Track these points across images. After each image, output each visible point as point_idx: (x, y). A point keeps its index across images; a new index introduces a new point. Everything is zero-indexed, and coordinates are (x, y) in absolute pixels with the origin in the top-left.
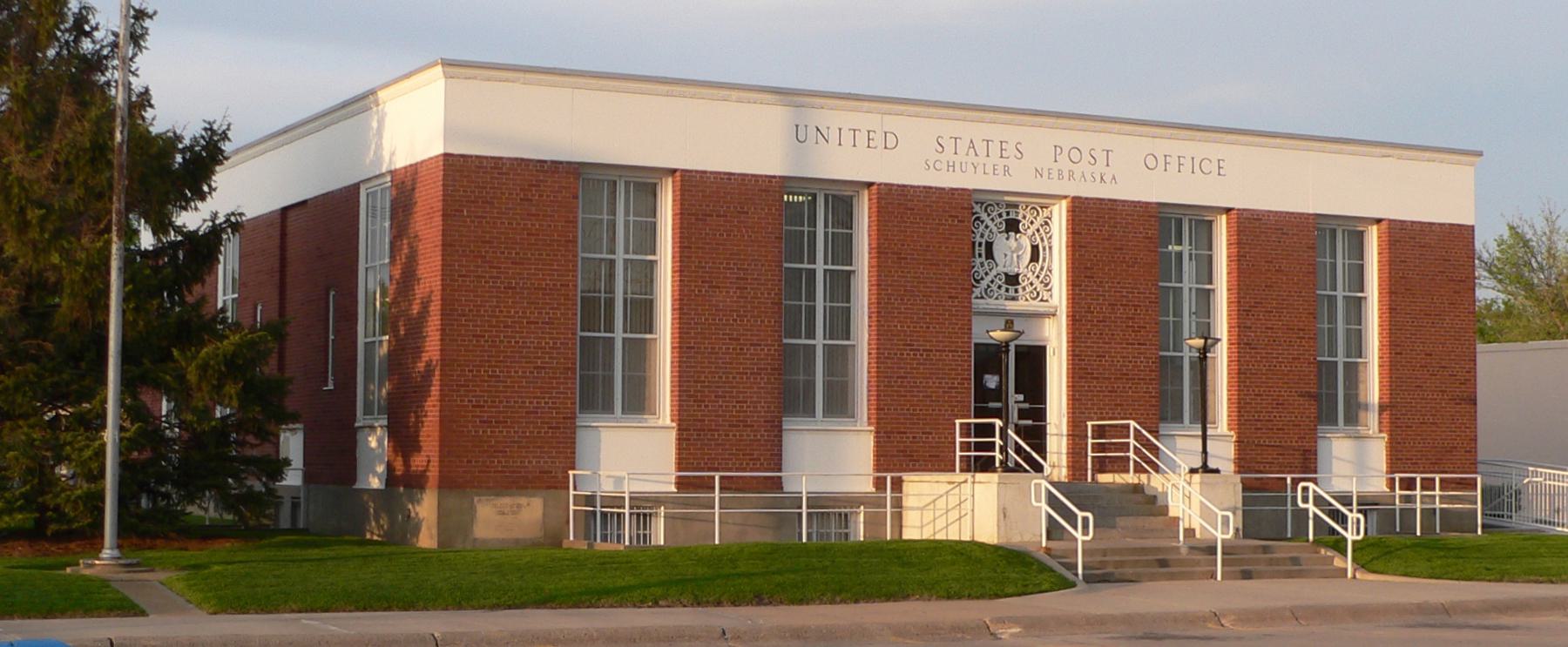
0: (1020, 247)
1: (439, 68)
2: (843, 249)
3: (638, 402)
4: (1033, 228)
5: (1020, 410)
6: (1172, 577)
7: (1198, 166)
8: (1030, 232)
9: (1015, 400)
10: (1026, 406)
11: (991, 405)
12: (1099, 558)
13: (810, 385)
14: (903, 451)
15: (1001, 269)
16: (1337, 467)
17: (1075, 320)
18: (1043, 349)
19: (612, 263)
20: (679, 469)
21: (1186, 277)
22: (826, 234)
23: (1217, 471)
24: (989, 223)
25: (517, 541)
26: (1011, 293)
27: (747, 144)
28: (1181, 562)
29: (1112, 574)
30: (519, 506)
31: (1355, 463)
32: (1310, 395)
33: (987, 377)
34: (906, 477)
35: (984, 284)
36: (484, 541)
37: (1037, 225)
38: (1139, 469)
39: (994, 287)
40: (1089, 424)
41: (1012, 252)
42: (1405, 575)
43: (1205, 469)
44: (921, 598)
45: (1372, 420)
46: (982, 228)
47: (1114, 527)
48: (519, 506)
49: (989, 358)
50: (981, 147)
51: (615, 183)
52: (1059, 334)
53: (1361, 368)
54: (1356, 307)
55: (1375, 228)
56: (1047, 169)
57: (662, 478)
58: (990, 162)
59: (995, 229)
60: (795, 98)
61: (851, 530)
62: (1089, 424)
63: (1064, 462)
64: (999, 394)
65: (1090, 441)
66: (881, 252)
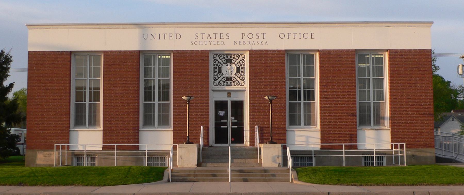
0: (232, 68)
3: (309, 122)
4: (237, 61)
8: (236, 63)
9: (230, 119)
10: (236, 121)
12: (188, 173)
15: (224, 76)
16: (367, 140)
20: (321, 143)
27: (127, 41)
30: (51, 154)
31: (376, 139)
36: (39, 165)
37: (239, 60)
39: (221, 82)
41: (229, 70)
45: (387, 123)
48: (51, 154)
49: (220, 105)
50: (213, 36)
53: (381, 104)
55: (387, 53)
56: (165, 42)
58: (259, 40)
59: (222, 63)
64: (225, 117)
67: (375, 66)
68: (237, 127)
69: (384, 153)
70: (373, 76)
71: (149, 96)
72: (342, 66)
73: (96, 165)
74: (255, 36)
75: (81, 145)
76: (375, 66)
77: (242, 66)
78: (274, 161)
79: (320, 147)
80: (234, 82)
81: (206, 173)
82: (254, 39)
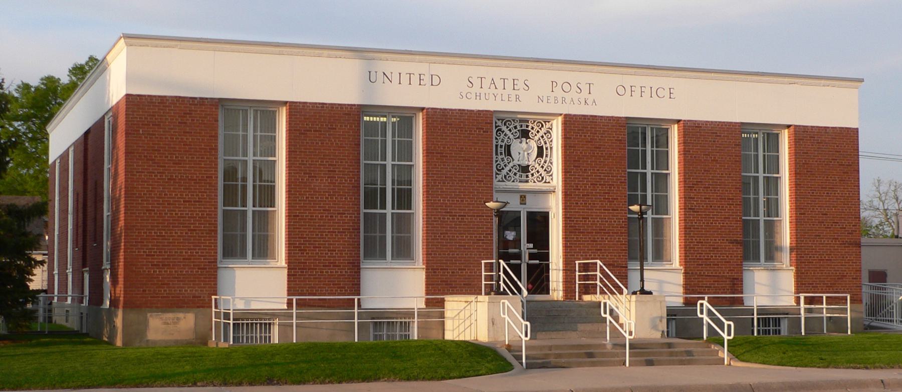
0: (529, 148)
1: (122, 40)
2: (662, 160)
3: (263, 250)
4: (539, 135)
5: (530, 254)
6: (593, 364)
7: (655, 93)
8: (536, 138)
9: (526, 247)
10: (535, 251)
11: (511, 251)
13: (383, 239)
14: (445, 281)
15: (516, 162)
16: (758, 289)
17: (567, 195)
18: (548, 213)
19: (384, 167)
21: (649, 165)
22: (393, 142)
23: (650, 293)
24: (508, 132)
25: (176, 342)
26: (524, 178)
28: (604, 355)
29: (550, 362)
31: (771, 287)
32: (737, 242)
33: (507, 232)
34: (448, 298)
35: (504, 172)
37: (542, 133)
38: (602, 292)
39: (511, 174)
40: (577, 262)
41: (524, 151)
42: (764, 363)
43: (643, 292)
44: (388, 380)
45: (786, 257)
46: (502, 135)
47: (576, 330)
48: (178, 319)
50: (499, 84)
51: (247, 110)
52: (557, 204)
54: (772, 184)
56: (547, 97)
57: (279, 300)
59: (511, 137)
60: (366, 54)
61: (410, 333)
62: (577, 262)
63: (561, 288)
64: (517, 242)
65: (577, 274)
66: (429, 153)
67: (396, 139)
68: (537, 262)
69: (785, 312)
70: (393, 160)
71: (233, 194)
72: (723, 154)
73: (276, 340)
74: (574, 88)
75: (242, 299)
76: (396, 139)
77: (548, 145)
78: (655, 327)
79: (448, 305)
80: (532, 175)
81: (571, 351)
82: (574, 94)
